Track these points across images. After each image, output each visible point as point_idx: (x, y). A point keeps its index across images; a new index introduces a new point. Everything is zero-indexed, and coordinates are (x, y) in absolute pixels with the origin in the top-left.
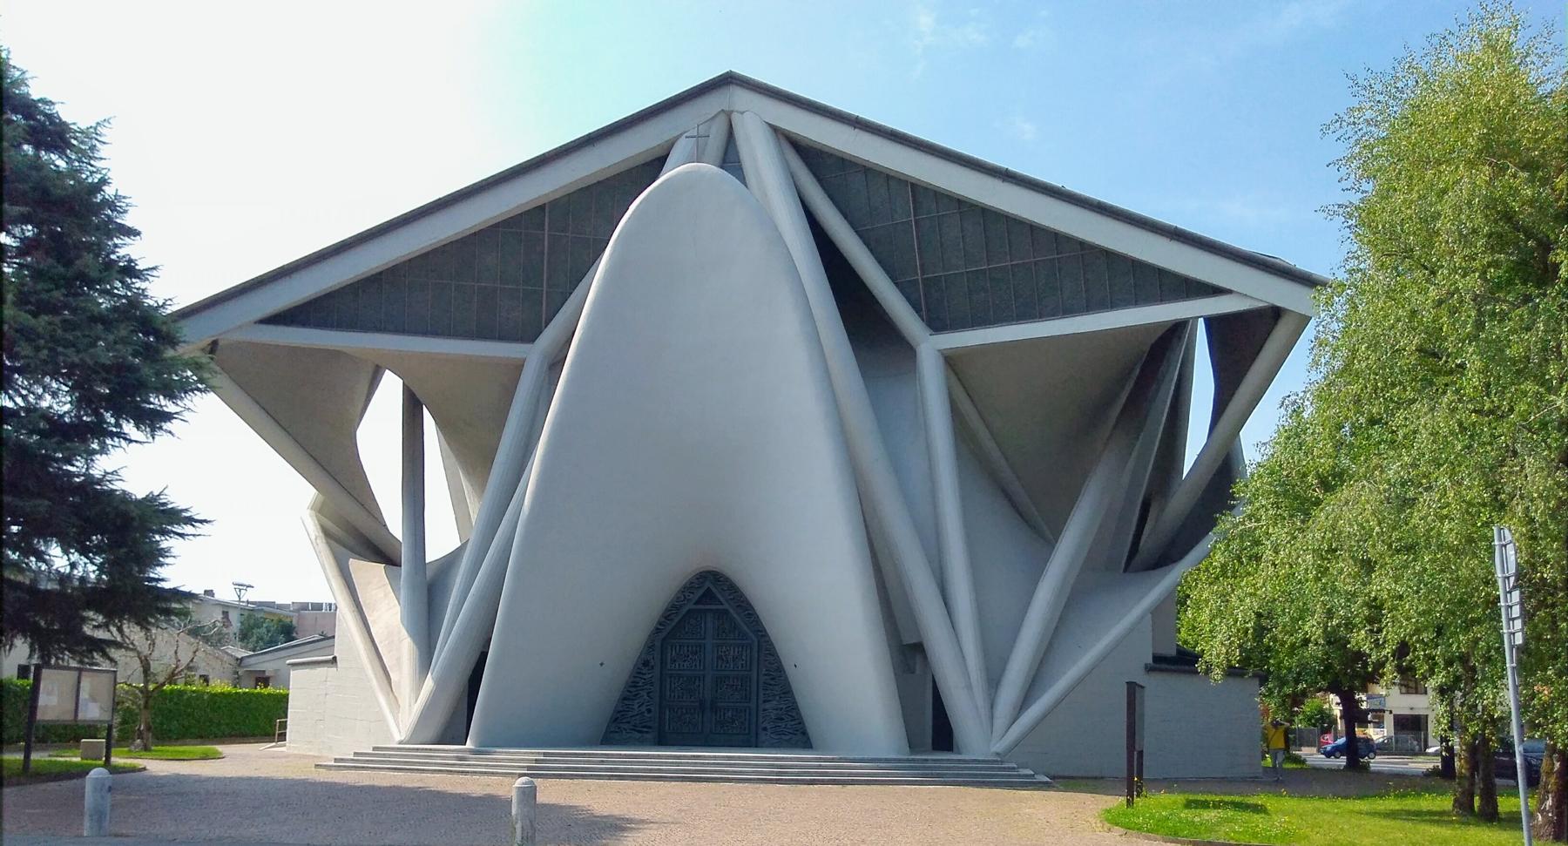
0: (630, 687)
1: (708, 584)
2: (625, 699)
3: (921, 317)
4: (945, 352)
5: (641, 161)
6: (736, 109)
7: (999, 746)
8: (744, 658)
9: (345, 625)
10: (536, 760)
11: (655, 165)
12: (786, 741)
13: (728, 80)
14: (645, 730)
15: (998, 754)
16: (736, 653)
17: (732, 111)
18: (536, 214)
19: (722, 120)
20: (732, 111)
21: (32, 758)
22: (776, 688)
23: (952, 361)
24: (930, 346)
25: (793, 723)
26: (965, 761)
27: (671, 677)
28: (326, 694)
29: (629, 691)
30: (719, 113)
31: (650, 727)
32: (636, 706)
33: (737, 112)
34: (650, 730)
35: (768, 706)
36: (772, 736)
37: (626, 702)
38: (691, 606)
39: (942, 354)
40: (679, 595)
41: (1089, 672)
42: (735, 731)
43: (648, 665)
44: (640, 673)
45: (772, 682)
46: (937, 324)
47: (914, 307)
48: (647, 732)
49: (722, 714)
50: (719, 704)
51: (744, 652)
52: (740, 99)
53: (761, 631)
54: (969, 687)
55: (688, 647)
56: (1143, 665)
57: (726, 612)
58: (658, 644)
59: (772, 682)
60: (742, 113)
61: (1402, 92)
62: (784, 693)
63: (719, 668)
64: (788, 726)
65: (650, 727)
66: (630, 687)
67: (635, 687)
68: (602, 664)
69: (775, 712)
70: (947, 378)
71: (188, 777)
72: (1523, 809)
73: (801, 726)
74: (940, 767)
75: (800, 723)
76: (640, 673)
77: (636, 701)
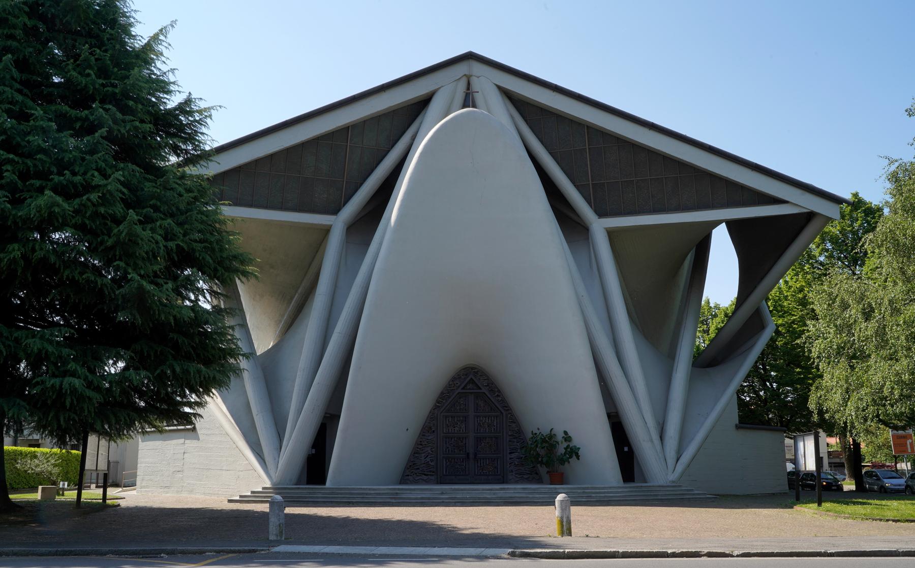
3: (591, 207)
4: (608, 229)
5: (413, 102)
6: (474, 74)
7: (672, 477)
8: (495, 425)
10: (584, 492)
11: (423, 104)
13: (470, 57)
15: (673, 482)
16: (490, 420)
17: (471, 76)
18: (345, 131)
19: (464, 80)
20: (471, 76)
23: (612, 234)
24: (599, 226)
26: (650, 486)
28: (184, 453)
30: (462, 76)
32: (423, 458)
33: (474, 76)
35: (513, 456)
36: (517, 475)
37: (416, 455)
39: (607, 230)
40: (451, 383)
41: (711, 431)
42: (491, 473)
46: (601, 213)
47: (587, 202)
48: (432, 475)
49: (482, 462)
51: (495, 420)
52: (477, 68)
53: (506, 407)
54: (651, 441)
56: (734, 425)
60: (478, 77)
61: (889, 373)
63: (479, 431)
68: (407, 430)
70: (584, 223)
71: (249, 511)
72: (107, 54)
74: (317, 497)
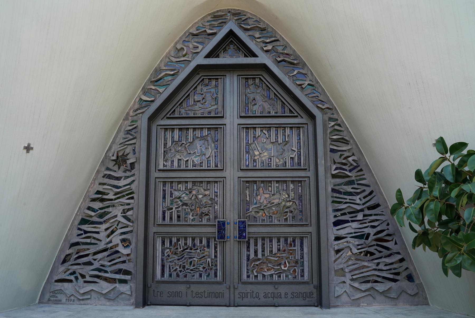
0: (93, 200)
1: (231, 25)
2: (84, 221)
9: (374, 305)
12: (383, 293)
14: (118, 276)
21: (429, 238)
22: (357, 199)
25: (388, 260)
27: (164, 183)
29: (89, 208)
31: (127, 272)
32: (102, 236)
34: (127, 277)
37: (85, 227)
38: (200, 60)
43: (125, 161)
44: (110, 177)
45: (349, 189)
50: (252, 230)
55: (186, 239)
57: (264, 67)
58: (143, 123)
59: (349, 189)
62: (369, 208)
64: (381, 267)
65: (127, 272)
66: (93, 200)
67: (102, 200)
68: (28, 148)
69: (357, 242)
73: (404, 264)
75: (402, 260)
76: (110, 177)
77: (104, 226)
